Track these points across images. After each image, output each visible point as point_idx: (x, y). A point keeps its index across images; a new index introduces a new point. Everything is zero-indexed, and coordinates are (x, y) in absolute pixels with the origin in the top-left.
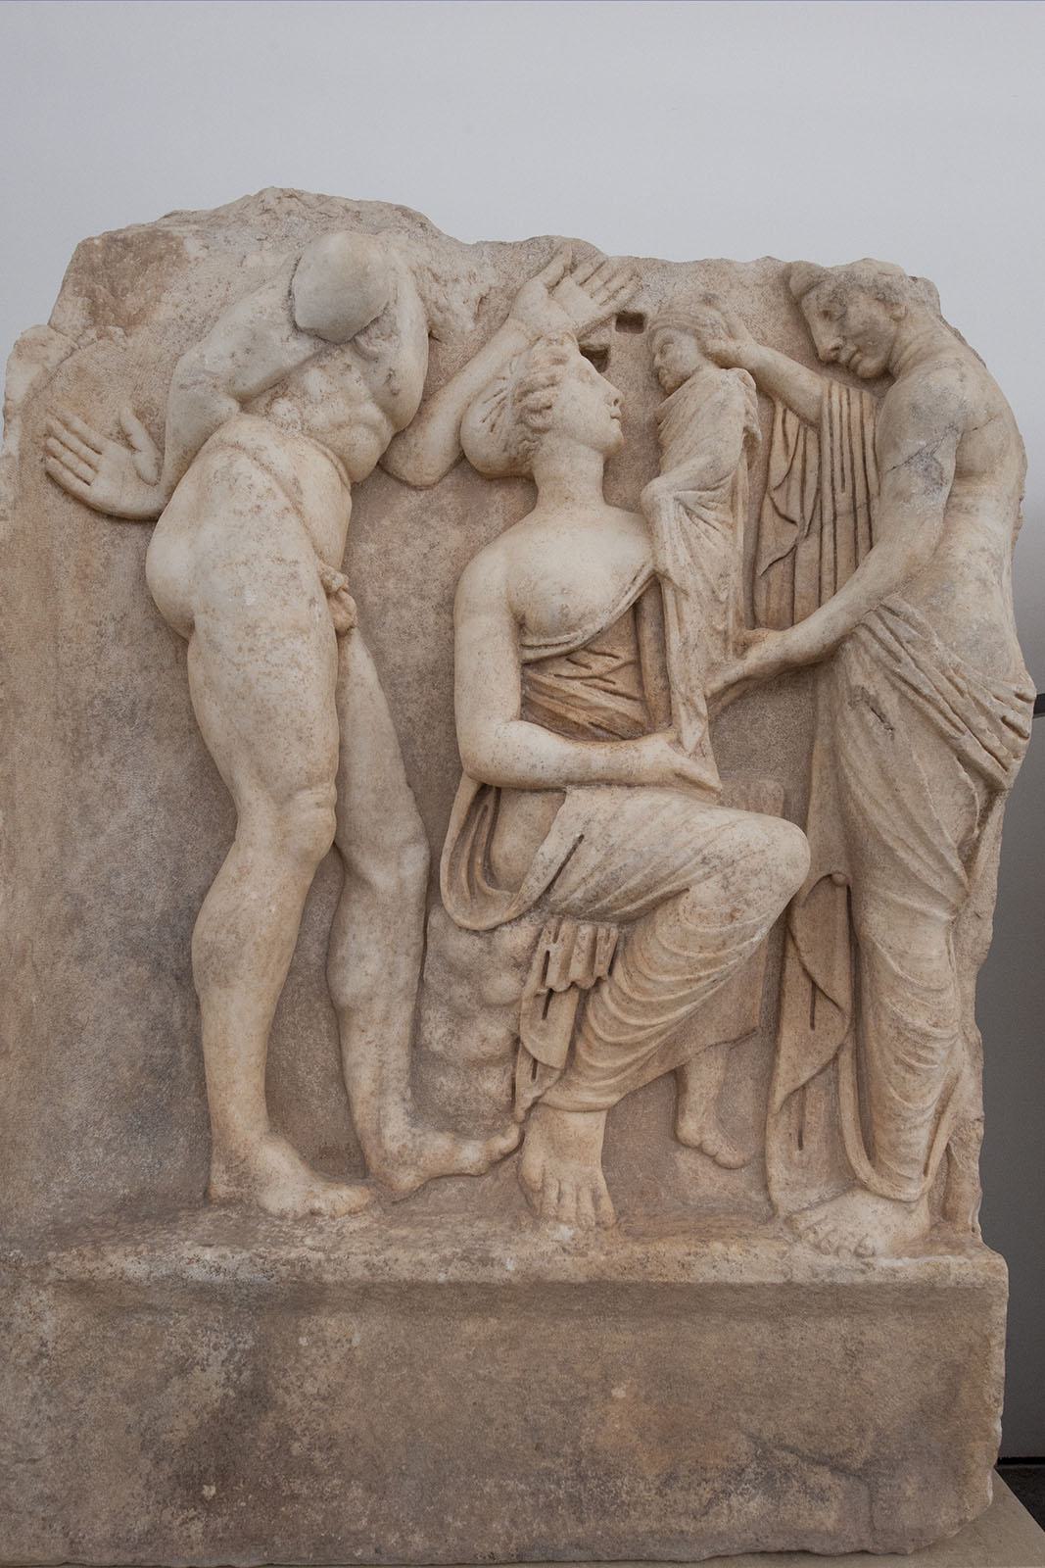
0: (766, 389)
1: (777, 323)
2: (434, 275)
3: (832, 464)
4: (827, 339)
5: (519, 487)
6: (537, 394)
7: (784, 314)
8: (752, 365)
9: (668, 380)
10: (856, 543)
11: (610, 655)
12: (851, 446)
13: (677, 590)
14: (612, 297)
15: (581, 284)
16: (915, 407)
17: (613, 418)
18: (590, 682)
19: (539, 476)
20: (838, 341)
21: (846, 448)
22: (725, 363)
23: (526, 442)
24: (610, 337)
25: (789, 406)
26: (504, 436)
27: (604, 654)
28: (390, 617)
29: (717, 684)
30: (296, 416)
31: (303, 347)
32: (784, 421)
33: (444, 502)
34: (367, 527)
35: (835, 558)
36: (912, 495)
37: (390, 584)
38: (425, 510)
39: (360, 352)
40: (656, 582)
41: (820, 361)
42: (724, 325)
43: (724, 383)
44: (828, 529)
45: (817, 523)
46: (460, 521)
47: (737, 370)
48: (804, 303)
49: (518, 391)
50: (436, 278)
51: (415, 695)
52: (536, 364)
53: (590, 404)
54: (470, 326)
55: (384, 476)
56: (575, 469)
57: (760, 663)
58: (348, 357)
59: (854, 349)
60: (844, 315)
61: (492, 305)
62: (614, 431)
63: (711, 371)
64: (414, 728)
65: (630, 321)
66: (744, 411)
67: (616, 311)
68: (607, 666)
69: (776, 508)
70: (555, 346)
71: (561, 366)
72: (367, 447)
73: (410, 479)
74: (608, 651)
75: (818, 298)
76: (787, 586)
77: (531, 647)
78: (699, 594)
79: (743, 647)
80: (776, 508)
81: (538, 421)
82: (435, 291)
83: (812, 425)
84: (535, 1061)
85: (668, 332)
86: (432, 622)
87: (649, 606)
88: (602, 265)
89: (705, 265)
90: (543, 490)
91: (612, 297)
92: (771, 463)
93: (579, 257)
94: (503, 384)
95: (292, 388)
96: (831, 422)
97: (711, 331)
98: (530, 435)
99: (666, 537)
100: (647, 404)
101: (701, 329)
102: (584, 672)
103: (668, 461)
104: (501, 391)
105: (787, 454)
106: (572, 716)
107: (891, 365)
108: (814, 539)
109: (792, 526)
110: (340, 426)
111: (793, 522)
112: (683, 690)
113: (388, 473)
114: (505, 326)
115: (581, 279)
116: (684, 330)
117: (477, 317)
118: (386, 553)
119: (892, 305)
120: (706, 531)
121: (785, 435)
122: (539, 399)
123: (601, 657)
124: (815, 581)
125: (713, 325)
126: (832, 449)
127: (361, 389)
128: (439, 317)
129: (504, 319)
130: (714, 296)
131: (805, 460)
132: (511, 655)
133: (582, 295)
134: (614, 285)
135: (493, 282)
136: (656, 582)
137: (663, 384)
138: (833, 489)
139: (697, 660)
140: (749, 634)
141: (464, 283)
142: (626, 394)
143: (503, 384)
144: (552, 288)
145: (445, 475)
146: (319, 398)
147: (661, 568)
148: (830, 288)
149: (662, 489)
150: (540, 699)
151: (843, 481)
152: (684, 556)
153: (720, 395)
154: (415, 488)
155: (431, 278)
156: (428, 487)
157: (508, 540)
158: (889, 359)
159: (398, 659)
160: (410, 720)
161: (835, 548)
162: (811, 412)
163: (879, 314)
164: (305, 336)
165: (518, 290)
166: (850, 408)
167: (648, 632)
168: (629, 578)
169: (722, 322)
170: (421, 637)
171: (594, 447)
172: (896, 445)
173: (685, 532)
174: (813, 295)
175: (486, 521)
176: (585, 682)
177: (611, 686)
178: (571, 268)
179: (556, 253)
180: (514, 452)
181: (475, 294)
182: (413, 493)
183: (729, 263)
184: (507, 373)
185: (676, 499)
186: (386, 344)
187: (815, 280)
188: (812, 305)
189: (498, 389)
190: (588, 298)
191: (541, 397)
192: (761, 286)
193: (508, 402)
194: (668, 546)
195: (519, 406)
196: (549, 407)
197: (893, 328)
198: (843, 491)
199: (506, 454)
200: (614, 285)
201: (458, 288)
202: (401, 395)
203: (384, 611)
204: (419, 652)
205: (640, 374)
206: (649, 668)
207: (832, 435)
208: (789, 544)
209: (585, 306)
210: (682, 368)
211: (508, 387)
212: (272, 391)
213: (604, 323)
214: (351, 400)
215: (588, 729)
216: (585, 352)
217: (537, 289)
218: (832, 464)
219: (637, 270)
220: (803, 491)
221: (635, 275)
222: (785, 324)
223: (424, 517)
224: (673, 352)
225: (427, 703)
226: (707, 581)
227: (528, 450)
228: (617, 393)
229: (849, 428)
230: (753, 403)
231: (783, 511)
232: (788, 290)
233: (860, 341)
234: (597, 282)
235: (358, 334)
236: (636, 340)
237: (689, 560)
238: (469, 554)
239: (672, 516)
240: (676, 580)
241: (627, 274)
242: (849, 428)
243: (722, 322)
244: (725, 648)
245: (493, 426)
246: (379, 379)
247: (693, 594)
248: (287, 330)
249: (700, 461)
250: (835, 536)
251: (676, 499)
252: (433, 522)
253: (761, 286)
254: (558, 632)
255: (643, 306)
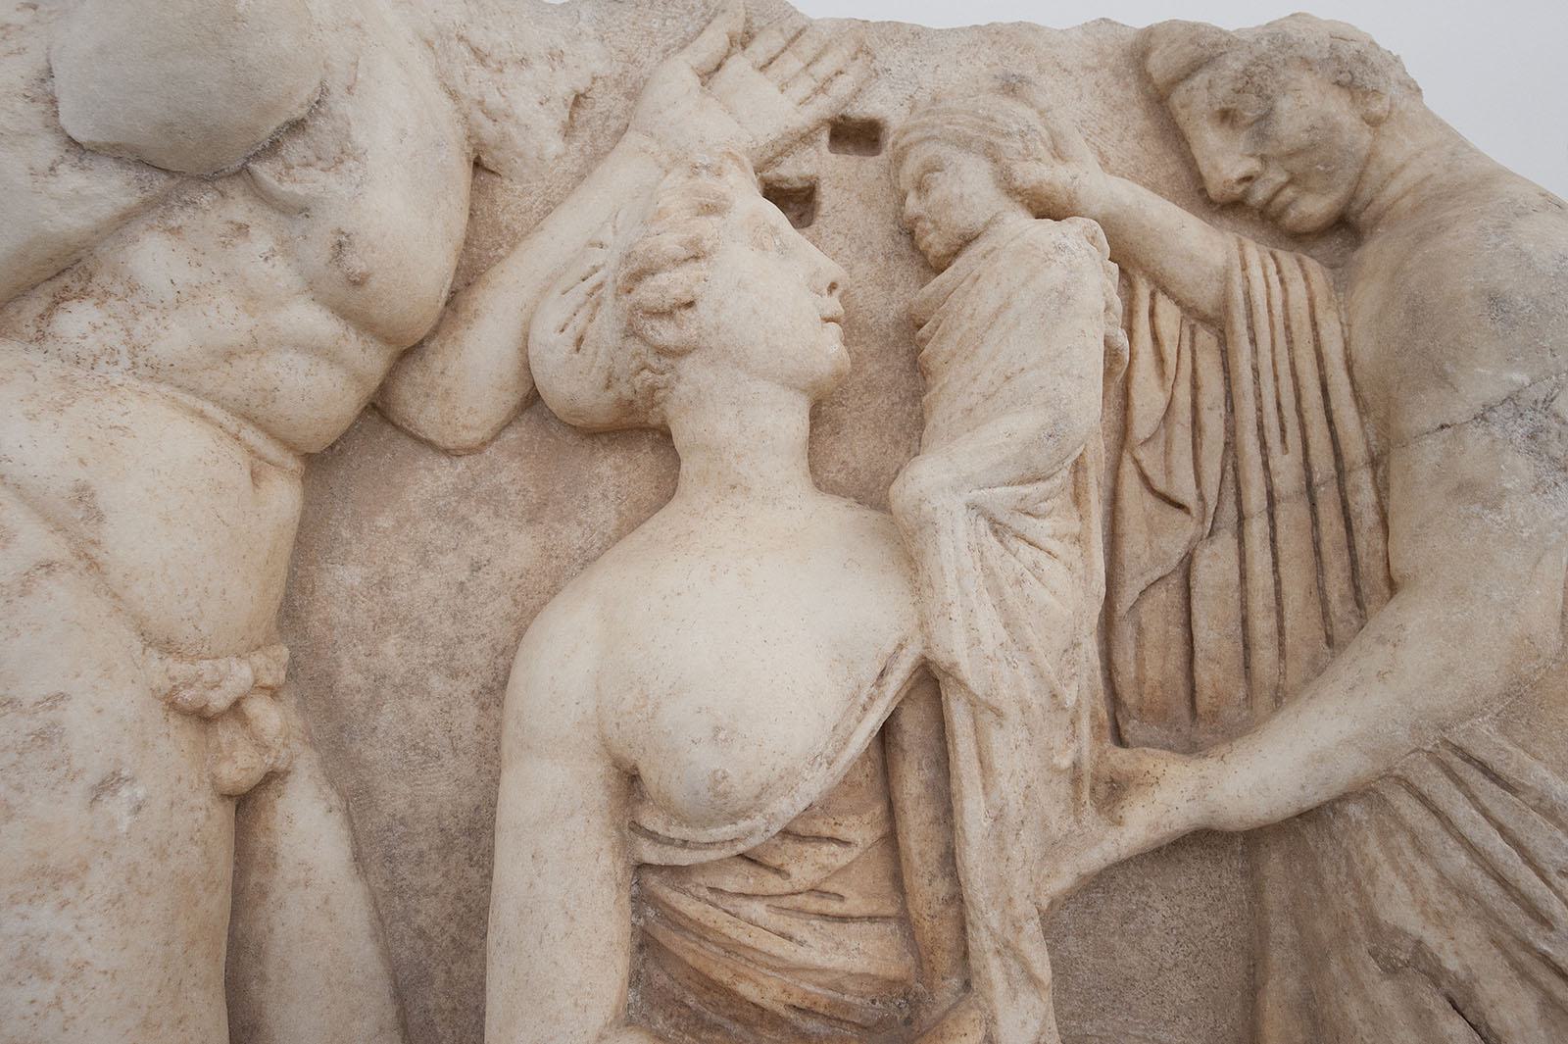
0: (1129, 259)
1: (1129, 130)
2: (475, 51)
3: (1259, 396)
4: (1227, 161)
5: (647, 449)
6: (662, 279)
7: (1138, 119)
8: (1096, 209)
9: (934, 242)
10: (1318, 552)
11: (831, 839)
12: (1293, 364)
13: (974, 703)
14: (822, 89)
15: (762, 68)
16: (1495, 300)
17: (828, 320)
18: (786, 902)
19: (683, 434)
20: (1251, 165)
21: (1284, 368)
22: (1047, 208)
23: (646, 373)
24: (820, 163)
25: (1161, 286)
26: (602, 359)
27: (818, 838)
28: (388, 716)
29: (1063, 881)
30: (114, 337)
31: (108, 190)
32: (1152, 314)
33: (504, 478)
34: (346, 534)
35: (1278, 583)
36: (1503, 494)
37: (390, 647)
38: (465, 494)
39: (263, 197)
40: (930, 681)
41: (1209, 202)
42: (1045, 134)
43: (1060, 249)
44: (1257, 528)
45: (1230, 512)
46: (533, 517)
47: (1079, 220)
48: (1178, 97)
49: (624, 271)
50: (480, 57)
51: (434, 879)
52: (660, 214)
53: (778, 299)
54: (555, 145)
55: (388, 430)
56: (744, 425)
57: (1155, 836)
58: (239, 208)
59: (1283, 178)
60: (1266, 117)
61: (600, 107)
62: (828, 350)
63: (1020, 224)
64: (430, 953)
65: (856, 134)
66: (1103, 307)
67: (828, 115)
68: (824, 867)
69: (1145, 479)
70: (705, 180)
71: (715, 219)
72: (321, 391)
73: (433, 437)
74: (826, 831)
75: (1210, 86)
76: (1177, 632)
77: (653, 836)
78: (1025, 708)
79: (1113, 792)
80: (1145, 479)
81: (666, 333)
82: (478, 82)
83: (1206, 320)
84: (785, 833)
85: (929, 151)
86: (470, 726)
87: (914, 728)
88: (800, 33)
89: (993, 34)
90: (689, 466)
91: (822, 89)
92: (1134, 394)
93: (757, 22)
94: (598, 257)
95: (103, 279)
96: (1250, 314)
97: (1019, 145)
98: (652, 361)
99: (952, 593)
100: (892, 286)
101: (1001, 141)
102: (773, 884)
103: (943, 412)
104: (595, 269)
105: (1162, 374)
106: (745, 989)
107: (1356, 207)
108: (1226, 542)
109: (1179, 515)
110: (229, 355)
111: (1180, 506)
112: (995, 924)
113: (397, 428)
114: (620, 146)
115: (762, 60)
116: (965, 144)
117: (568, 131)
118: (384, 584)
119: (1366, 94)
120: (1036, 565)
121: (1156, 338)
122: (666, 290)
123: (808, 849)
124: (1234, 626)
125: (1023, 135)
126: (1256, 370)
127: (281, 274)
128: (489, 131)
129: (620, 134)
130: (1022, 79)
131: (1195, 387)
132: (606, 861)
133: (765, 88)
134: (823, 69)
135: (599, 67)
136: (930, 681)
137: (926, 252)
138: (1264, 445)
139: (1025, 847)
140: (1120, 759)
141: (541, 68)
142: (850, 268)
143: (598, 257)
144: (709, 74)
145: (508, 424)
146: (171, 297)
147: (940, 656)
148: (1238, 66)
149: (934, 480)
150: (675, 942)
151: (1283, 430)
152: (989, 624)
153: (1055, 275)
154: (446, 452)
155: (468, 56)
156: (470, 451)
157: (610, 578)
158: (1353, 198)
159: (401, 804)
160: (421, 933)
161: (1276, 564)
162: (1206, 298)
163: (1340, 109)
164: (109, 164)
165: (646, 82)
166: (1285, 290)
167: (913, 781)
168: (869, 671)
169: (1040, 128)
170: (447, 756)
171: (789, 383)
172: (1443, 379)
173: (990, 573)
174: (1200, 80)
175: (582, 516)
176: (776, 902)
177: (835, 907)
178: (744, 40)
179: (715, 15)
180: (626, 391)
181: (563, 87)
182: (445, 461)
183: (1034, 29)
184: (607, 236)
185: (972, 506)
186: (331, 180)
187: (1203, 52)
188: (1196, 100)
189: (587, 268)
190: (775, 91)
191: (670, 284)
192: (1094, 70)
193: (608, 293)
194: (956, 612)
195: (627, 301)
196: (690, 304)
197: (1366, 138)
198: (1285, 450)
199: (611, 394)
200: (823, 69)
201: (528, 75)
202: (373, 284)
203: (374, 705)
204: (443, 788)
205: (878, 231)
206: (917, 861)
207: (1253, 341)
208: (1178, 552)
209: (773, 107)
210: (962, 219)
211: (608, 263)
212: (50, 287)
213: (806, 138)
214: (253, 299)
215: (785, 1021)
216: (775, 193)
217: (677, 78)
218: (1259, 396)
219: (866, 42)
220: (1196, 446)
221: (863, 50)
222: (1140, 137)
223: (463, 510)
224: (944, 187)
225: (459, 898)
226: (1040, 675)
227: (653, 389)
228: (833, 270)
229: (1288, 328)
230: (1114, 285)
231: (1160, 485)
232: (1144, 77)
233: (1297, 164)
234: (791, 64)
235: (257, 157)
236: (870, 166)
237: (1003, 635)
238: (547, 583)
239: (963, 546)
240: (976, 684)
241: (847, 51)
242: (1288, 328)
243: (1040, 128)
244: (1076, 799)
245: (580, 340)
246: (317, 253)
247: (1013, 712)
248: (46, 149)
249: (1024, 424)
250: (1273, 541)
251: (972, 506)
252: (479, 520)
253: (1094, 70)
254: (710, 822)
255: (879, 106)
